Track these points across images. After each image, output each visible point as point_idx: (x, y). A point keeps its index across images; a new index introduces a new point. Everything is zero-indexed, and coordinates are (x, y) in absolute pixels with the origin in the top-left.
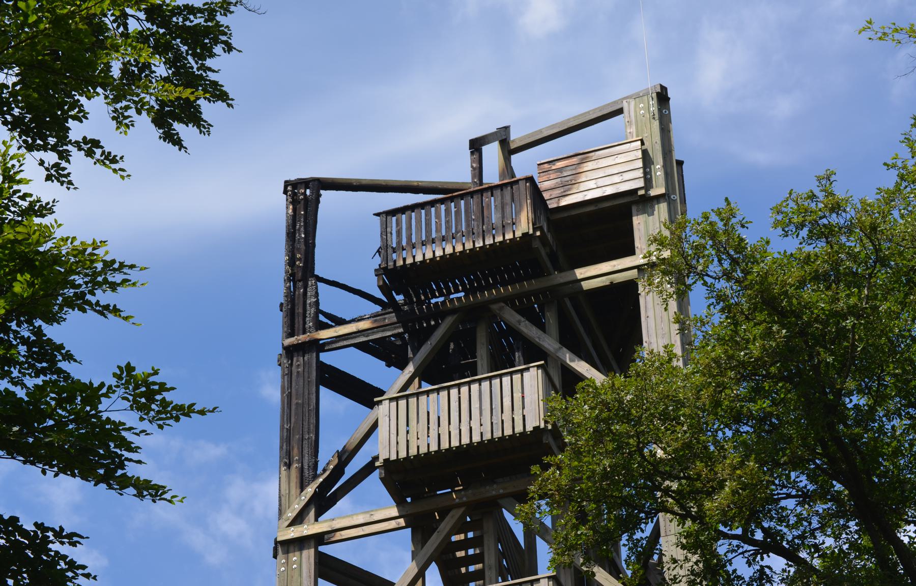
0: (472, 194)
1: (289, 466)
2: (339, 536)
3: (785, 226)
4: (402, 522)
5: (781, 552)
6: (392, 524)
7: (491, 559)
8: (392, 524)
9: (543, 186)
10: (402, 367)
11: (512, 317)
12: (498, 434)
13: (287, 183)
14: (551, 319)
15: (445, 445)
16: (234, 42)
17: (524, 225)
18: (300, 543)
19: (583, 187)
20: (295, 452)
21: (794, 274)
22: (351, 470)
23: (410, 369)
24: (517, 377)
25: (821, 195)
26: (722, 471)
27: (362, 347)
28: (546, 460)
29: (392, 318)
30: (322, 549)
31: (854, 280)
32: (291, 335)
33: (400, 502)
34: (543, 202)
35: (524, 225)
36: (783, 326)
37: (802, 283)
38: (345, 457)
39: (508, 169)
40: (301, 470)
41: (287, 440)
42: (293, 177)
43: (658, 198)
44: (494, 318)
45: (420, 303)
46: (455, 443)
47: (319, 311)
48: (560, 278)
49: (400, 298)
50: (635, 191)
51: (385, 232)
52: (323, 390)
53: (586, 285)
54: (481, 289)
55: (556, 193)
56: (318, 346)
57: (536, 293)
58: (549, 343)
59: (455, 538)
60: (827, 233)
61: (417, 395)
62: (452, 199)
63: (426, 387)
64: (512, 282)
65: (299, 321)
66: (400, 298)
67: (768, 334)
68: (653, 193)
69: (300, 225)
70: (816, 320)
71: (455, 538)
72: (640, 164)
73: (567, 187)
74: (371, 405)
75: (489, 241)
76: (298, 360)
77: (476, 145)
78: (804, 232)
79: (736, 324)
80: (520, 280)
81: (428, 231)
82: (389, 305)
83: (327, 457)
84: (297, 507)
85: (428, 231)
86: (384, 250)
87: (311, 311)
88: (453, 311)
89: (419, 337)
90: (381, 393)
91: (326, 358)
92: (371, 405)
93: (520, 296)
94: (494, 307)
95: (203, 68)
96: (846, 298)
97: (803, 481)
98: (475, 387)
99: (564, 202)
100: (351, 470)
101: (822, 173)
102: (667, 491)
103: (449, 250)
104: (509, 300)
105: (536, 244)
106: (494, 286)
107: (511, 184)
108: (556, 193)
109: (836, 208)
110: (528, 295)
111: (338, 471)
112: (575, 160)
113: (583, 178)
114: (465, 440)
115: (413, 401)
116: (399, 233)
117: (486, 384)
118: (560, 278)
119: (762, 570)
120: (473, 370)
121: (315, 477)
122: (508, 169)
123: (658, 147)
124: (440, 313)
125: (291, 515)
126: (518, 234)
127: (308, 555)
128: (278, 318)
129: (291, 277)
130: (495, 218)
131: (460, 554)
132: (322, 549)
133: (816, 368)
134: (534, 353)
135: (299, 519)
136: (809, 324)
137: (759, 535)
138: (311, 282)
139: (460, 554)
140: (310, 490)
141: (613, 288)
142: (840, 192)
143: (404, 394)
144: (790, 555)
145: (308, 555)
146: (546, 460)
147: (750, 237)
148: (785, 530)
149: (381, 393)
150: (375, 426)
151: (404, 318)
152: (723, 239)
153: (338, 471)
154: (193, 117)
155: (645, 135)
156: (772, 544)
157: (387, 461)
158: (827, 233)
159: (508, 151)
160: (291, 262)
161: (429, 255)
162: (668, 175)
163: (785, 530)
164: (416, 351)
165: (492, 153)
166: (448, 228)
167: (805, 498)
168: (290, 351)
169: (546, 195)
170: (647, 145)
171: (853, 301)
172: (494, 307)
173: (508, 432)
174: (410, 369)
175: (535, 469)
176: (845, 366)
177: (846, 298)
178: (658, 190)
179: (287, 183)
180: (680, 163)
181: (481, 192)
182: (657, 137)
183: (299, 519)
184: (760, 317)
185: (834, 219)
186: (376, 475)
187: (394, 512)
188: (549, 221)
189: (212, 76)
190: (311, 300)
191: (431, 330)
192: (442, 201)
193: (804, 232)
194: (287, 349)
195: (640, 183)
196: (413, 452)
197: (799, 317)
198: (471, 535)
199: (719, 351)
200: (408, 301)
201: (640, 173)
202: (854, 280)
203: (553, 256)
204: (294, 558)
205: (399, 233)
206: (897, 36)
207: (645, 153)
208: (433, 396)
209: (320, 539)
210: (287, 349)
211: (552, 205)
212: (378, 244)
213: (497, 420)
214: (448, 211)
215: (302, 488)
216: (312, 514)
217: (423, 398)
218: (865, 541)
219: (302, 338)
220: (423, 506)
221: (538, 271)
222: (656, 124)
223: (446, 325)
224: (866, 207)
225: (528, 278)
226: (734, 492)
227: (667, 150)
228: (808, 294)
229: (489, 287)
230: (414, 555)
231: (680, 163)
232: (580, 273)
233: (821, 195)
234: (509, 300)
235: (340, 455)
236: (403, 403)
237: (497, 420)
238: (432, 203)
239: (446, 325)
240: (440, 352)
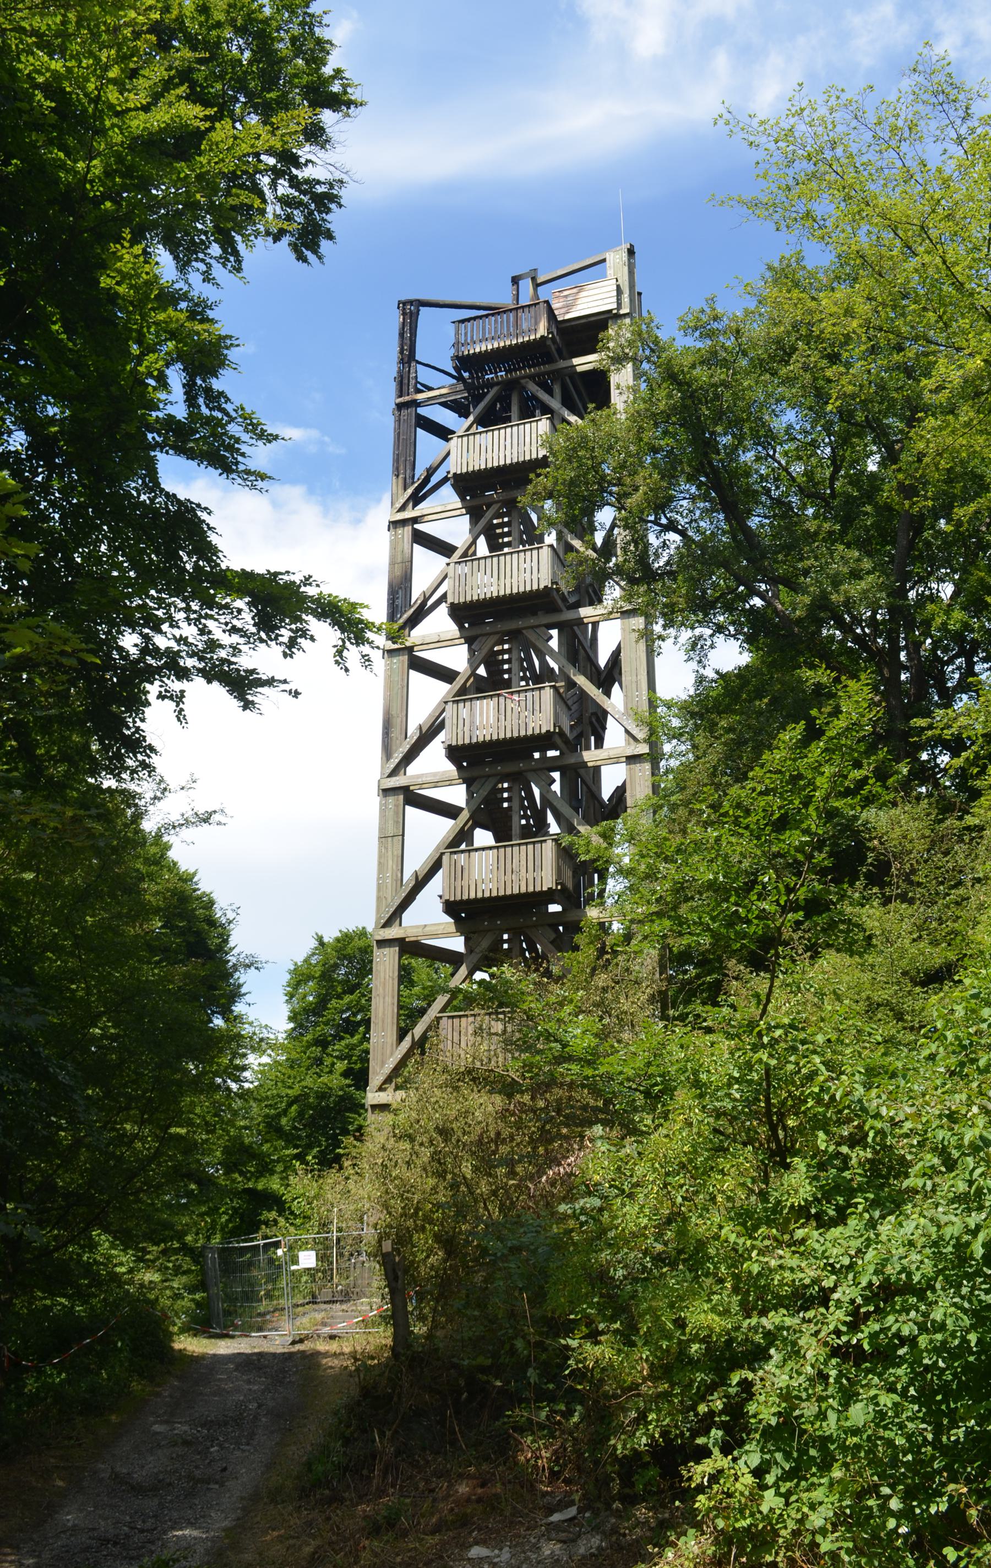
0: (511, 310)
1: (397, 476)
2: (426, 519)
3: (687, 330)
4: (464, 511)
5: (676, 531)
6: (458, 512)
7: (516, 534)
8: (458, 512)
9: (554, 306)
10: (466, 417)
11: (533, 388)
12: (521, 459)
13: (399, 302)
14: (557, 390)
15: (489, 465)
16: (342, 202)
17: (542, 330)
18: (403, 522)
19: (579, 307)
20: (401, 467)
21: (690, 359)
22: (434, 480)
23: (471, 418)
24: (534, 424)
25: (708, 310)
26: (639, 480)
27: (444, 404)
28: (539, 471)
29: (461, 387)
30: (416, 526)
31: (725, 364)
32: (400, 396)
33: (463, 499)
34: (555, 316)
35: (542, 330)
36: (679, 391)
37: (693, 366)
38: (431, 472)
39: (536, 296)
40: (405, 479)
41: (397, 460)
42: (403, 299)
43: (625, 315)
44: (524, 388)
45: (478, 378)
46: (496, 464)
47: (417, 382)
48: (562, 364)
49: (466, 375)
50: (610, 311)
51: (457, 333)
52: (419, 430)
53: (579, 369)
54: (515, 370)
55: (563, 311)
56: (415, 404)
57: (548, 373)
58: (555, 404)
59: (495, 522)
60: (711, 334)
61: (474, 434)
62: (499, 313)
63: (481, 429)
64: (534, 366)
65: (405, 388)
66: (466, 375)
67: (670, 396)
68: (622, 312)
69: (407, 328)
70: (701, 388)
71: (495, 522)
72: (615, 293)
73: (569, 307)
74: (447, 440)
75: (520, 340)
76: (404, 412)
77: (515, 280)
78: (697, 334)
79: (652, 389)
80: (538, 364)
81: (484, 333)
82: (460, 378)
83: (420, 472)
84: (402, 501)
85: (484, 333)
86: (456, 345)
87: (412, 382)
88: (498, 383)
89: (477, 399)
90: (453, 432)
91: (421, 411)
92: (447, 440)
93: (538, 375)
94: (523, 381)
95: (324, 220)
96: (720, 375)
97: (693, 490)
98: (509, 430)
99: (568, 317)
100: (434, 480)
101: (709, 296)
102: (611, 493)
103: (496, 345)
104: (532, 377)
105: (549, 343)
106: (524, 368)
107: (535, 305)
108: (563, 311)
109: (716, 318)
110: (543, 374)
111: (427, 480)
112: (575, 291)
113: (579, 302)
114: (502, 463)
115: (471, 438)
116: (466, 334)
117: (515, 429)
118: (562, 364)
119: (664, 542)
120: (509, 419)
121: (413, 483)
122: (536, 296)
123: (627, 283)
124: (490, 385)
125: (398, 506)
126: (538, 336)
127: (408, 530)
128: (392, 387)
129: (402, 361)
130: (525, 326)
131: (499, 531)
132: (416, 526)
133: (698, 418)
134: (546, 410)
135: (403, 508)
136: (696, 391)
137: (664, 521)
138: (413, 364)
139: (499, 531)
140: (410, 491)
141: (593, 372)
142: (720, 310)
143: (468, 433)
144: (682, 533)
145: (408, 530)
146: (539, 471)
147: (663, 335)
148: (679, 518)
149: (453, 432)
150: (448, 454)
151: (468, 387)
152: (646, 336)
153: (427, 480)
154: (314, 248)
155: (619, 276)
156: (671, 526)
157: (455, 474)
158: (711, 334)
159: (537, 285)
160: (401, 352)
161: (484, 348)
162: (632, 301)
163: (679, 518)
164: (475, 408)
165: (526, 287)
166: (496, 331)
167: (693, 499)
168: (400, 406)
169: (556, 312)
170: (620, 282)
171: (723, 376)
172: (523, 381)
173: (527, 458)
174: (471, 418)
175: (532, 476)
176: (719, 416)
177: (720, 375)
178: (625, 310)
179: (399, 302)
180: (640, 294)
181: (517, 309)
182: (626, 277)
183: (403, 508)
184: (665, 385)
185: (715, 325)
186: (448, 483)
187: (460, 505)
188: (558, 328)
189: (328, 226)
190: (413, 375)
191: (485, 395)
192: (493, 315)
193: (697, 334)
194: (398, 405)
195: (615, 306)
196: (471, 469)
197: (690, 386)
198: (506, 519)
199: (642, 406)
200: (471, 377)
201: (615, 299)
202: (725, 364)
203: (559, 351)
204: (400, 531)
205: (466, 334)
206: (731, 203)
207: (618, 287)
208: (484, 435)
209: (415, 520)
210: (398, 405)
211: (560, 319)
212: (453, 341)
213: (521, 451)
214: (496, 321)
215: (405, 490)
216: (411, 505)
217: (477, 436)
218: (726, 527)
219: (407, 398)
220: (477, 502)
221: (550, 359)
222: (626, 268)
223: (493, 392)
224: (734, 319)
225: (544, 364)
226: (645, 494)
227: (632, 286)
228: (697, 372)
229: (520, 369)
230: (471, 531)
231: (640, 294)
232: (576, 361)
233: (708, 310)
234: (532, 377)
235: (428, 470)
236: (465, 439)
237: (521, 451)
238: (487, 316)
239: (493, 392)
240: (490, 408)
